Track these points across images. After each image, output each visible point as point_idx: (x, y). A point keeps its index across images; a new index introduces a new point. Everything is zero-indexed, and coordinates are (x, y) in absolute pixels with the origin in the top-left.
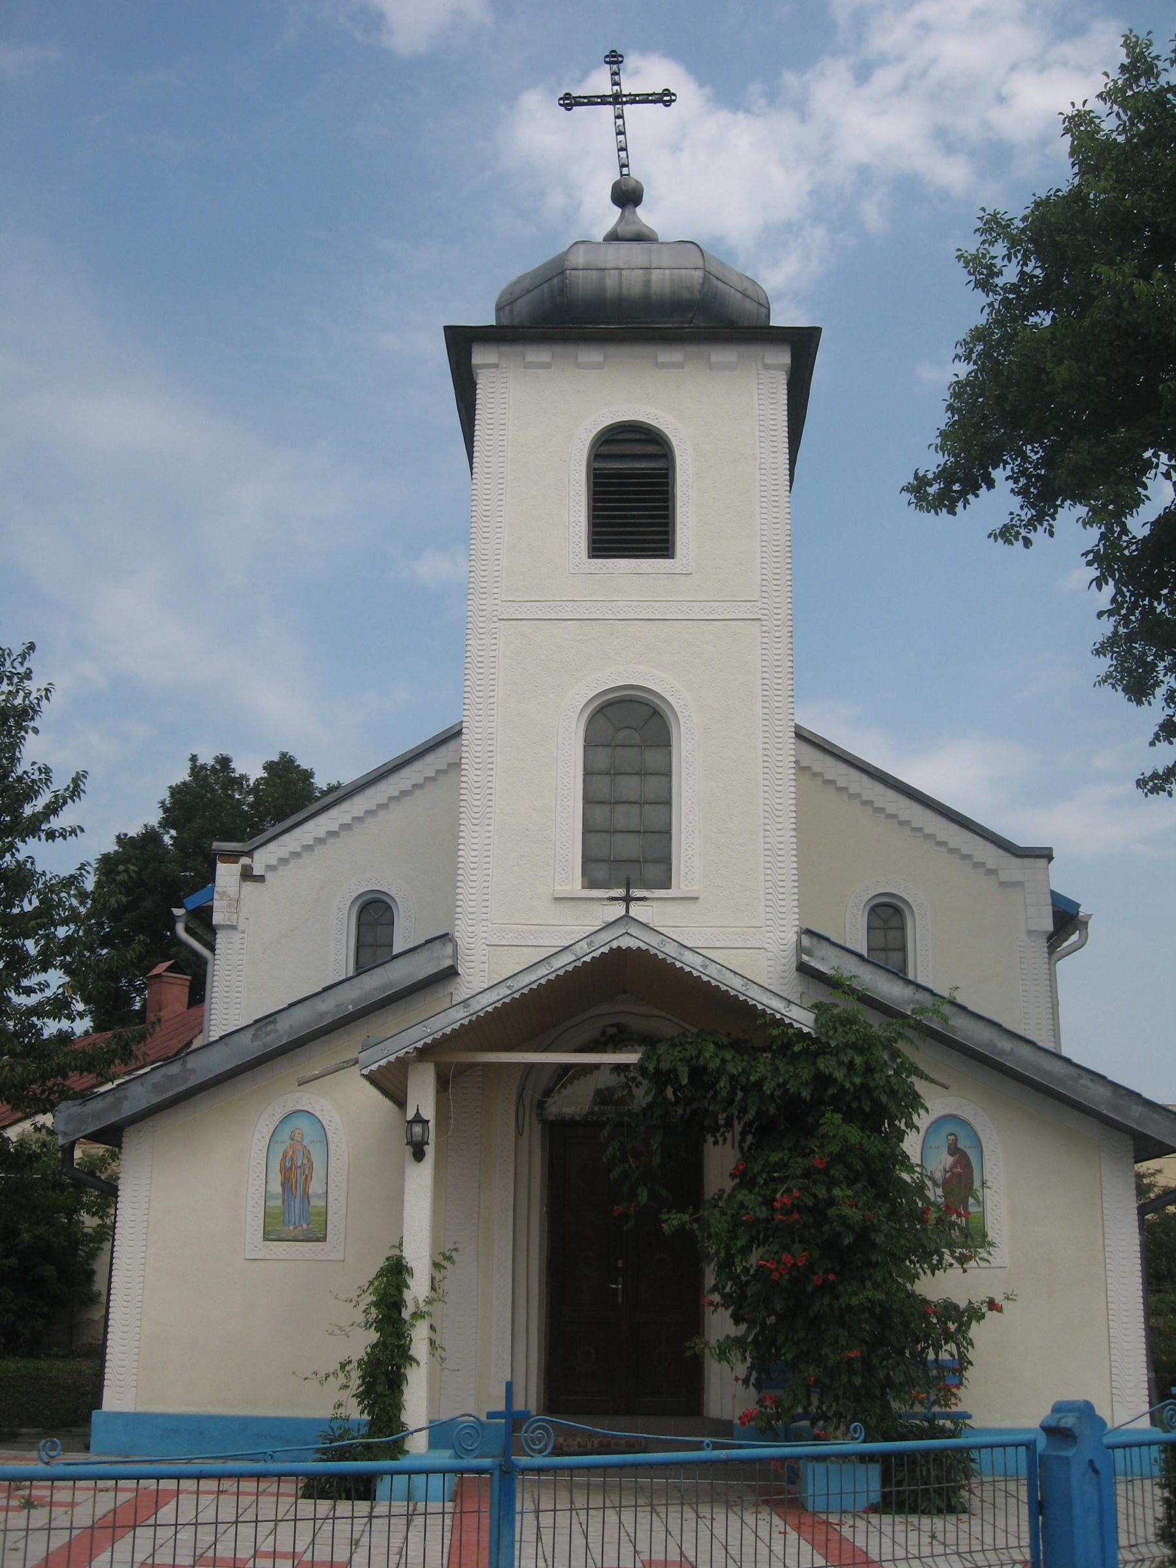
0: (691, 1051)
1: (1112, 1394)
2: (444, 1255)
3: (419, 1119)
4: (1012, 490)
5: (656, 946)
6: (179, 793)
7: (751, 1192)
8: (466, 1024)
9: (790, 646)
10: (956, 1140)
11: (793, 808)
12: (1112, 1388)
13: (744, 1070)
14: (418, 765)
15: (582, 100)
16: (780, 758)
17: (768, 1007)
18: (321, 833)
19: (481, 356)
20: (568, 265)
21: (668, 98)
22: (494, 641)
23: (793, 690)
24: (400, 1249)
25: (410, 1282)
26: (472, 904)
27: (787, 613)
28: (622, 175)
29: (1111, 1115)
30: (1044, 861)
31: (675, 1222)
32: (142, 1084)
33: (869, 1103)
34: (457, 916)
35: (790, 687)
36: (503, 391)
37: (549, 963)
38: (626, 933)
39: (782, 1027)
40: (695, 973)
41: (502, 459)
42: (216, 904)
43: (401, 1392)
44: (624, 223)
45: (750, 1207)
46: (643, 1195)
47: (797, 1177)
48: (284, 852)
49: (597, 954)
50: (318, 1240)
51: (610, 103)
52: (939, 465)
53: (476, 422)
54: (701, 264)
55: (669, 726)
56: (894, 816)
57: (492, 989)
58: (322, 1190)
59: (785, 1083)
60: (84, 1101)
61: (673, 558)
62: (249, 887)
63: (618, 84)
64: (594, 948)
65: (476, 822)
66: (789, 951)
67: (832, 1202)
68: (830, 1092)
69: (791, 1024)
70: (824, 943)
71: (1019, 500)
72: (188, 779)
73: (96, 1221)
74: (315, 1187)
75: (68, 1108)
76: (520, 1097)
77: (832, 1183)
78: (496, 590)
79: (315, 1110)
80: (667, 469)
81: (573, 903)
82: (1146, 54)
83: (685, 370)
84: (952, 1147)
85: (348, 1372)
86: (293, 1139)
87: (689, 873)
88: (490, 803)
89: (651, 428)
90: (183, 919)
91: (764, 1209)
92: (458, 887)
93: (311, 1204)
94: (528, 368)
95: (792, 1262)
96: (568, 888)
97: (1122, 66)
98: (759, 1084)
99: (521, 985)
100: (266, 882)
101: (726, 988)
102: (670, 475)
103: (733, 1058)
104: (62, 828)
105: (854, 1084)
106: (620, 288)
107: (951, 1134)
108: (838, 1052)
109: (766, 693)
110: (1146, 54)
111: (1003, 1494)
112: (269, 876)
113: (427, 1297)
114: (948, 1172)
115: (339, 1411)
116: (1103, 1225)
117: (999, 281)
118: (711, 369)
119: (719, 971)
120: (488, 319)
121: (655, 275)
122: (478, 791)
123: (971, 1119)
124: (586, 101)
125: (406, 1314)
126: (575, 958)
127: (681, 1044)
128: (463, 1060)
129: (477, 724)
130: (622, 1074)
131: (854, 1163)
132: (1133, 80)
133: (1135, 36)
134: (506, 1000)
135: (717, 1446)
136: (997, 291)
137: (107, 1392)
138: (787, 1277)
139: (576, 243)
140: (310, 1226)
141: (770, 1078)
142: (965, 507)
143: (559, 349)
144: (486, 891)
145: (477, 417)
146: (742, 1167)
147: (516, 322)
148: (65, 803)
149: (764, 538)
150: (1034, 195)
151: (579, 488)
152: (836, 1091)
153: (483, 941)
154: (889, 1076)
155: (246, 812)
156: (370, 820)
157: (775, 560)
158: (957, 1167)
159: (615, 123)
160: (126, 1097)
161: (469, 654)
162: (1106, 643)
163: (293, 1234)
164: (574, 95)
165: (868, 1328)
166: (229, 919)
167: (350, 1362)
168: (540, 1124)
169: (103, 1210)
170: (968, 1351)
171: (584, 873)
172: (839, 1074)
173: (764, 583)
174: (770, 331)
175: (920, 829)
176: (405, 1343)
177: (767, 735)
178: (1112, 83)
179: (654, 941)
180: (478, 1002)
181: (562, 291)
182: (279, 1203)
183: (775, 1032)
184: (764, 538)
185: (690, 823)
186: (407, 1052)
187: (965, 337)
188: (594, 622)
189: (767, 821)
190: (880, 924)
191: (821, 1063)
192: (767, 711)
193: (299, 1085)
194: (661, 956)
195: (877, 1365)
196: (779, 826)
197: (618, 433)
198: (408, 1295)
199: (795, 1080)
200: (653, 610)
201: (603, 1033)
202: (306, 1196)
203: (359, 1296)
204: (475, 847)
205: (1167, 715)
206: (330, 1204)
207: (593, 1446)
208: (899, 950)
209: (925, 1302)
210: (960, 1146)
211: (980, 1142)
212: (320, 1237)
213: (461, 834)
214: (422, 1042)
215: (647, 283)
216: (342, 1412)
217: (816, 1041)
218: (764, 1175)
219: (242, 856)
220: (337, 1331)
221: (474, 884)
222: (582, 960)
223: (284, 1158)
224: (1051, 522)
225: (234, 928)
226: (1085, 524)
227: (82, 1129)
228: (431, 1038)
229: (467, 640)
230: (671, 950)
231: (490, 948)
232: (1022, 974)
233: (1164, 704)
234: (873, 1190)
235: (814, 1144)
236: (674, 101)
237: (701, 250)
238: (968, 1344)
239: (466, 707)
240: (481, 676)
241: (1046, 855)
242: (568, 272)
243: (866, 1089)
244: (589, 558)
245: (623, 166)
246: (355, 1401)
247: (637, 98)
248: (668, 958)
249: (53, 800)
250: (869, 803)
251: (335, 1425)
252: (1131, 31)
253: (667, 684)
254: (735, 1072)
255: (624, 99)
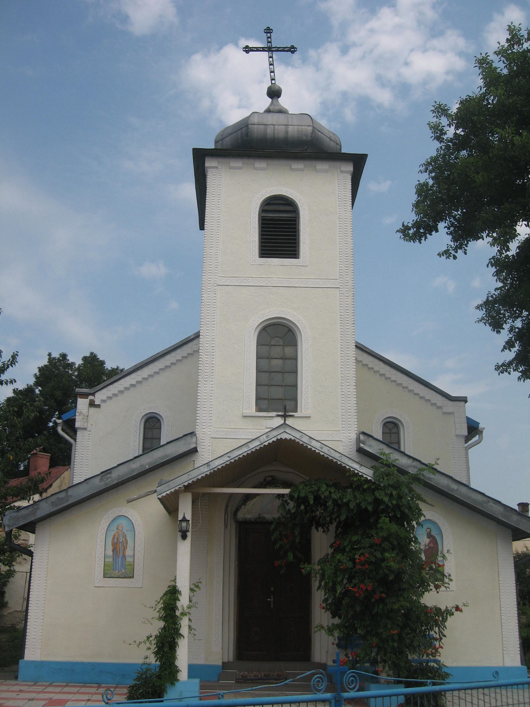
0: (315, 488)
1: (503, 650)
2: (195, 585)
3: (184, 520)
4: (447, 233)
5: (299, 438)
6: (43, 370)
7: (343, 554)
8: (208, 474)
9: (353, 300)
10: (431, 531)
11: (355, 376)
12: (503, 647)
13: (340, 497)
14: (173, 354)
15: (254, 49)
16: (348, 352)
17: (351, 467)
18: (128, 385)
19: (209, 163)
20: (250, 122)
21: (293, 50)
22: (215, 295)
23: (354, 321)
24: (175, 582)
25: (180, 597)
26: (204, 418)
27: (351, 285)
28: (272, 84)
29: (503, 519)
30: (463, 403)
31: (308, 569)
32: (46, 502)
33: (399, 513)
34: (197, 424)
35: (353, 320)
36: (220, 179)
37: (248, 446)
38: (285, 432)
39: (358, 477)
40: (317, 451)
41: (219, 211)
42: (77, 418)
43: (176, 651)
44: (273, 105)
45: (344, 562)
46: (290, 557)
47: (367, 548)
48: (110, 394)
49: (270, 441)
50: (130, 577)
51: (266, 51)
52: (413, 221)
53: (207, 193)
54: (311, 124)
55: (296, 337)
56: (395, 381)
57: (221, 458)
58: (132, 554)
59: (360, 503)
60: (18, 510)
61: (298, 259)
62: (93, 410)
63: (270, 42)
64: (269, 439)
65: (206, 380)
66: (353, 442)
67: (383, 560)
68: (381, 507)
69: (362, 476)
70: (371, 439)
71: (450, 237)
72: (46, 363)
73: (7, 568)
74: (129, 552)
75: (10, 513)
76: (226, 510)
77: (384, 551)
78: (216, 272)
79: (129, 515)
80: (295, 217)
81: (252, 419)
82: (518, 34)
83: (304, 172)
84: (429, 534)
85: (151, 641)
86: (118, 529)
87: (306, 405)
88: (213, 371)
89: (289, 199)
90: (61, 425)
91: (350, 563)
92: (197, 410)
93: (127, 560)
94: (231, 169)
95: (365, 588)
96: (249, 411)
97: (507, 39)
98: (347, 504)
99: (234, 456)
100: (101, 408)
101: (331, 458)
102: (297, 220)
103: (335, 491)
104: (6, 380)
105: (392, 504)
106: (274, 134)
107: (428, 528)
108: (385, 489)
109: (342, 322)
110: (518, 34)
111: (458, 698)
112: (102, 405)
113: (188, 605)
114: (427, 546)
115: (146, 661)
116: (498, 571)
117: (445, 137)
118: (316, 172)
119: (329, 450)
120: (212, 146)
121: (290, 128)
122: (207, 365)
123: (437, 521)
124: (255, 49)
125: (178, 613)
126: (260, 443)
127: (310, 485)
128: (205, 492)
129: (207, 334)
130: (281, 499)
131: (393, 541)
132: (511, 46)
133: (513, 26)
134: (223, 465)
135: (434, 684)
136: (444, 141)
137: (27, 651)
138: (363, 595)
139: (253, 113)
140: (126, 571)
141: (353, 500)
142: (425, 240)
143: (246, 161)
144: (210, 412)
145: (207, 191)
146: (338, 543)
147: (224, 148)
148: (8, 367)
149: (341, 250)
150: (460, 97)
151: (255, 225)
152: (384, 507)
153: (209, 436)
154: (409, 500)
155: (74, 379)
156: (150, 379)
157: (346, 260)
158: (431, 544)
159: (269, 60)
160: (38, 508)
161: (203, 301)
162: (483, 304)
163: (118, 575)
164: (250, 46)
165: (400, 619)
166: (83, 425)
167: (151, 636)
168: (235, 523)
169: (11, 563)
170: (444, 631)
171: (257, 404)
172: (386, 499)
173: (341, 271)
174: (341, 155)
175: (406, 388)
176: (178, 627)
177: (342, 341)
178: (501, 47)
179: (298, 435)
180: (214, 464)
181: (247, 134)
182: (111, 560)
183: (355, 479)
184: (341, 250)
185: (307, 382)
186: (180, 487)
187: (424, 162)
188: (262, 287)
189: (342, 381)
190: (388, 431)
191: (377, 494)
192: (342, 330)
193: (127, 503)
194: (301, 443)
195: (405, 637)
196: (348, 384)
197: (272, 200)
198: (179, 604)
199: (365, 502)
200: (289, 282)
201: (265, 480)
202: (124, 556)
203: (156, 605)
204: (206, 391)
205: (510, 337)
206: (135, 561)
207: (261, 676)
208: (396, 443)
209: (426, 606)
210: (432, 534)
211: (441, 532)
212: (131, 576)
213: (199, 385)
214: (187, 483)
215: (287, 132)
216: (148, 661)
217: (374, 483)
218: (349, 547)
219: (90, 395)
220: (147, 622)
221: (204, 409)
222: (264, 444)
223: (114, 538)
224: (466, 248)
225: (85, 429)
226: (491, 245)
227: (17, 523)
228: (191, 480)
229: (202, 294)
230: (305, 440)
231: (213, 439)
232: (453, 455)
233: (508, 333)
234: (402, 554)
235: (373, 532)
236: (296, 51)
237: (311, 117)
238: (444, 627)
239: (201, 326)
240: (209, 312)
241: (464, 400)
242: (250, 125)
243: (398, 506)
244: (259, 258)
245: (272, 79)
246: (153, 656)
247: (279, 49)
248: (304, 444)
249: (2, 366)
250: (383, 375)
251: (144, 667)
252: (512, 23)
253: (296, 317)
254: (336, 498)
255: (273, 49)
